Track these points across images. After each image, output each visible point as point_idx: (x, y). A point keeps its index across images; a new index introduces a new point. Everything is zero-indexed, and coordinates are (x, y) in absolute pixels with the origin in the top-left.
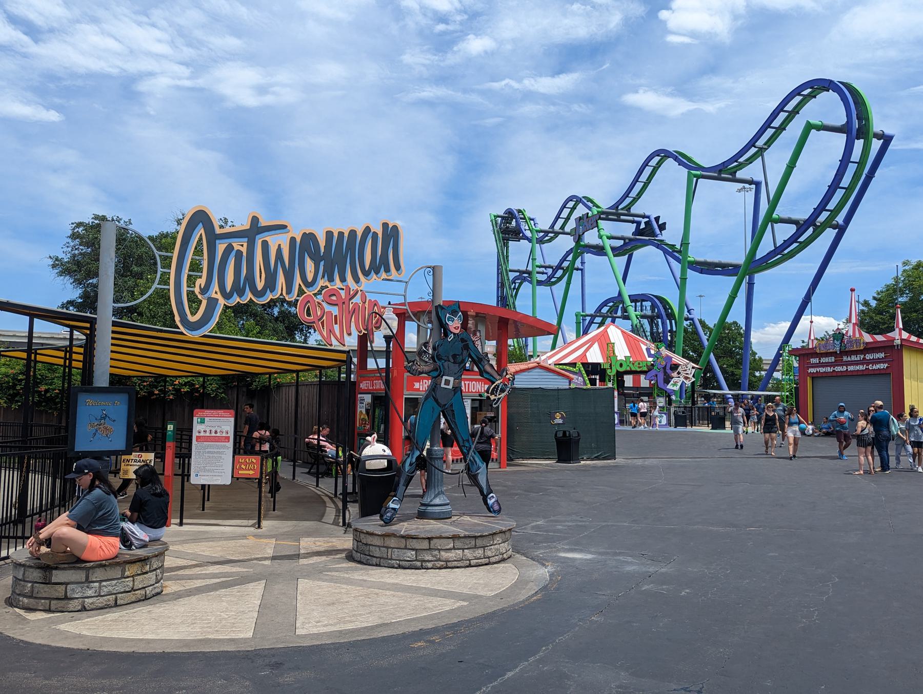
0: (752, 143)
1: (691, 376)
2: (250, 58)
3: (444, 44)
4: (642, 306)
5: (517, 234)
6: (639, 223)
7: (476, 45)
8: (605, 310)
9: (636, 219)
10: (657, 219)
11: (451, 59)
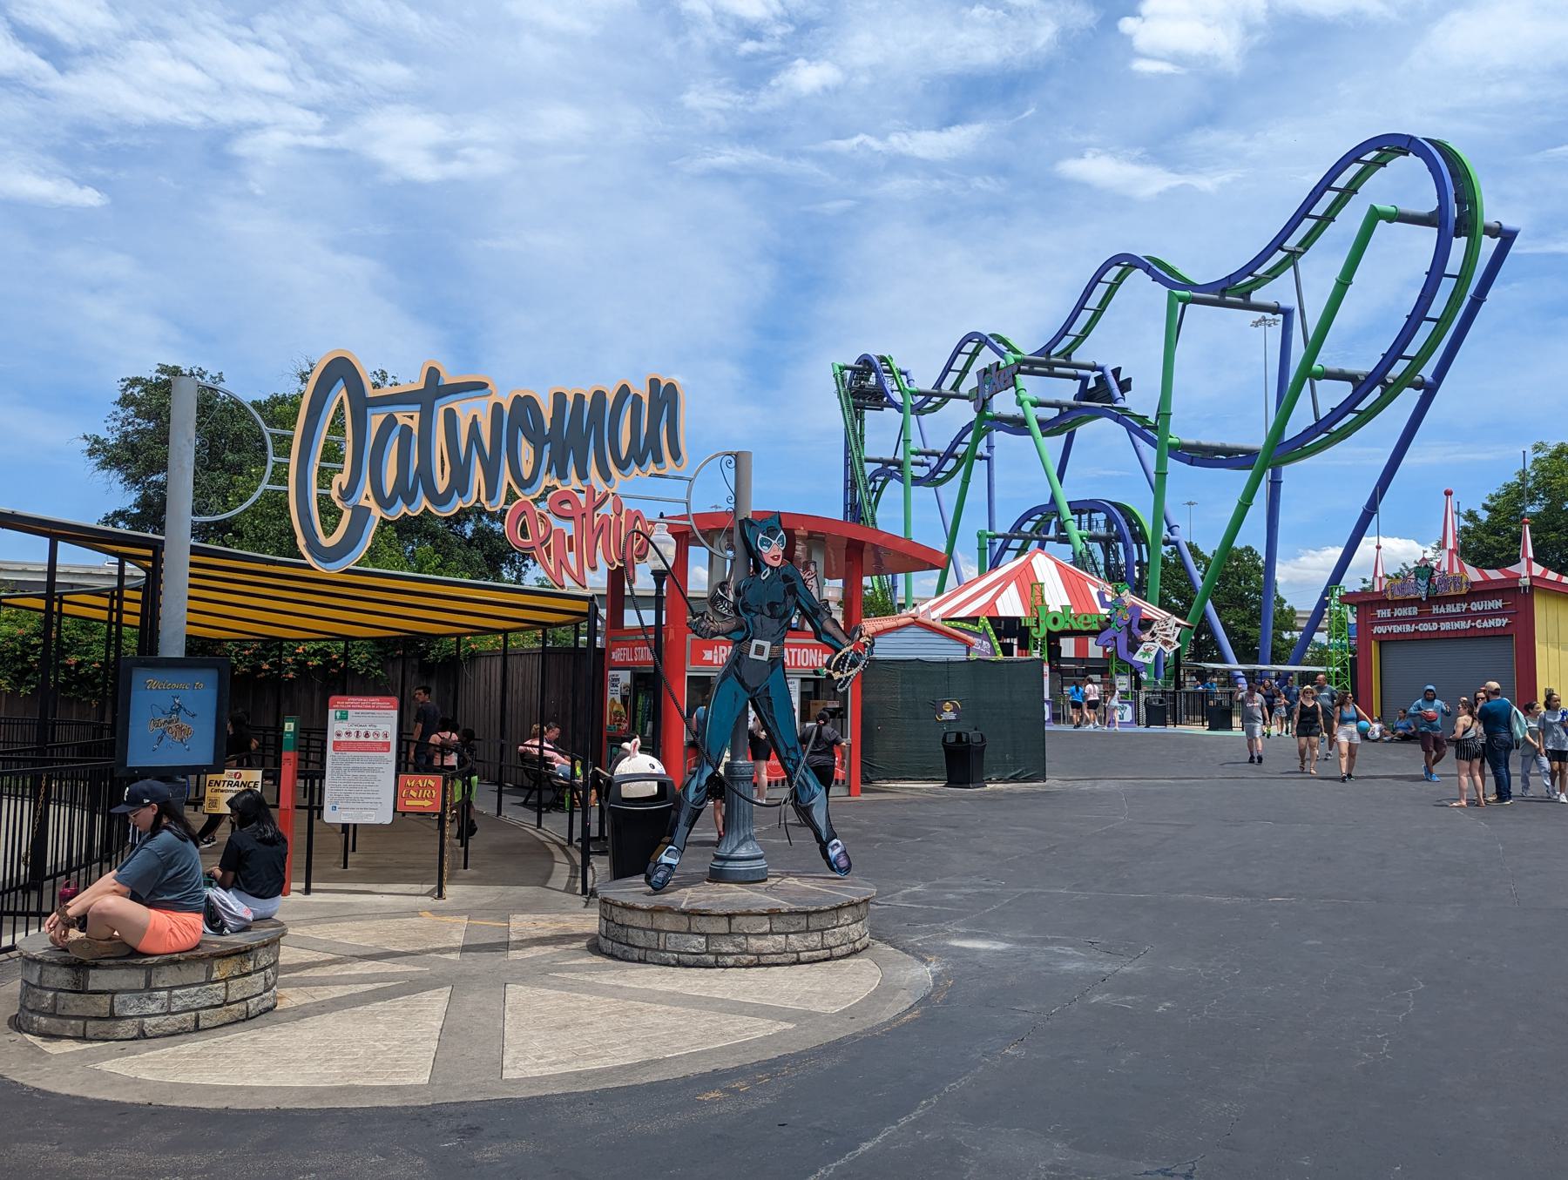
0: (1277, 244)
1: (1173, 640)
2: (424, 99)
3: (755, 75)
4: (1090, 520)
5: (878, 398)
6: (1085, 380)
7: (808, 76)
8: (1027, 527)
9: (1080, 372)
10: (1116, 372)
11: (767, 101)
